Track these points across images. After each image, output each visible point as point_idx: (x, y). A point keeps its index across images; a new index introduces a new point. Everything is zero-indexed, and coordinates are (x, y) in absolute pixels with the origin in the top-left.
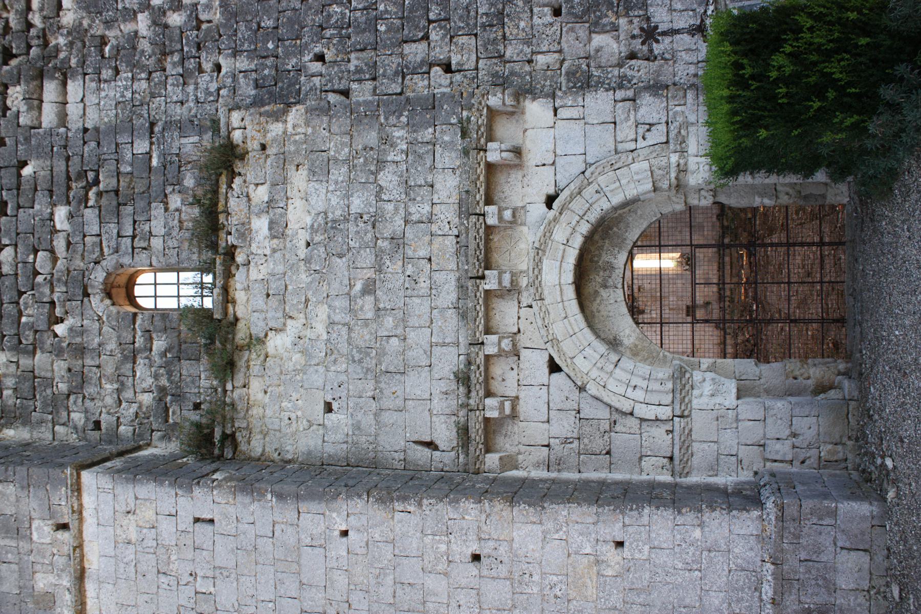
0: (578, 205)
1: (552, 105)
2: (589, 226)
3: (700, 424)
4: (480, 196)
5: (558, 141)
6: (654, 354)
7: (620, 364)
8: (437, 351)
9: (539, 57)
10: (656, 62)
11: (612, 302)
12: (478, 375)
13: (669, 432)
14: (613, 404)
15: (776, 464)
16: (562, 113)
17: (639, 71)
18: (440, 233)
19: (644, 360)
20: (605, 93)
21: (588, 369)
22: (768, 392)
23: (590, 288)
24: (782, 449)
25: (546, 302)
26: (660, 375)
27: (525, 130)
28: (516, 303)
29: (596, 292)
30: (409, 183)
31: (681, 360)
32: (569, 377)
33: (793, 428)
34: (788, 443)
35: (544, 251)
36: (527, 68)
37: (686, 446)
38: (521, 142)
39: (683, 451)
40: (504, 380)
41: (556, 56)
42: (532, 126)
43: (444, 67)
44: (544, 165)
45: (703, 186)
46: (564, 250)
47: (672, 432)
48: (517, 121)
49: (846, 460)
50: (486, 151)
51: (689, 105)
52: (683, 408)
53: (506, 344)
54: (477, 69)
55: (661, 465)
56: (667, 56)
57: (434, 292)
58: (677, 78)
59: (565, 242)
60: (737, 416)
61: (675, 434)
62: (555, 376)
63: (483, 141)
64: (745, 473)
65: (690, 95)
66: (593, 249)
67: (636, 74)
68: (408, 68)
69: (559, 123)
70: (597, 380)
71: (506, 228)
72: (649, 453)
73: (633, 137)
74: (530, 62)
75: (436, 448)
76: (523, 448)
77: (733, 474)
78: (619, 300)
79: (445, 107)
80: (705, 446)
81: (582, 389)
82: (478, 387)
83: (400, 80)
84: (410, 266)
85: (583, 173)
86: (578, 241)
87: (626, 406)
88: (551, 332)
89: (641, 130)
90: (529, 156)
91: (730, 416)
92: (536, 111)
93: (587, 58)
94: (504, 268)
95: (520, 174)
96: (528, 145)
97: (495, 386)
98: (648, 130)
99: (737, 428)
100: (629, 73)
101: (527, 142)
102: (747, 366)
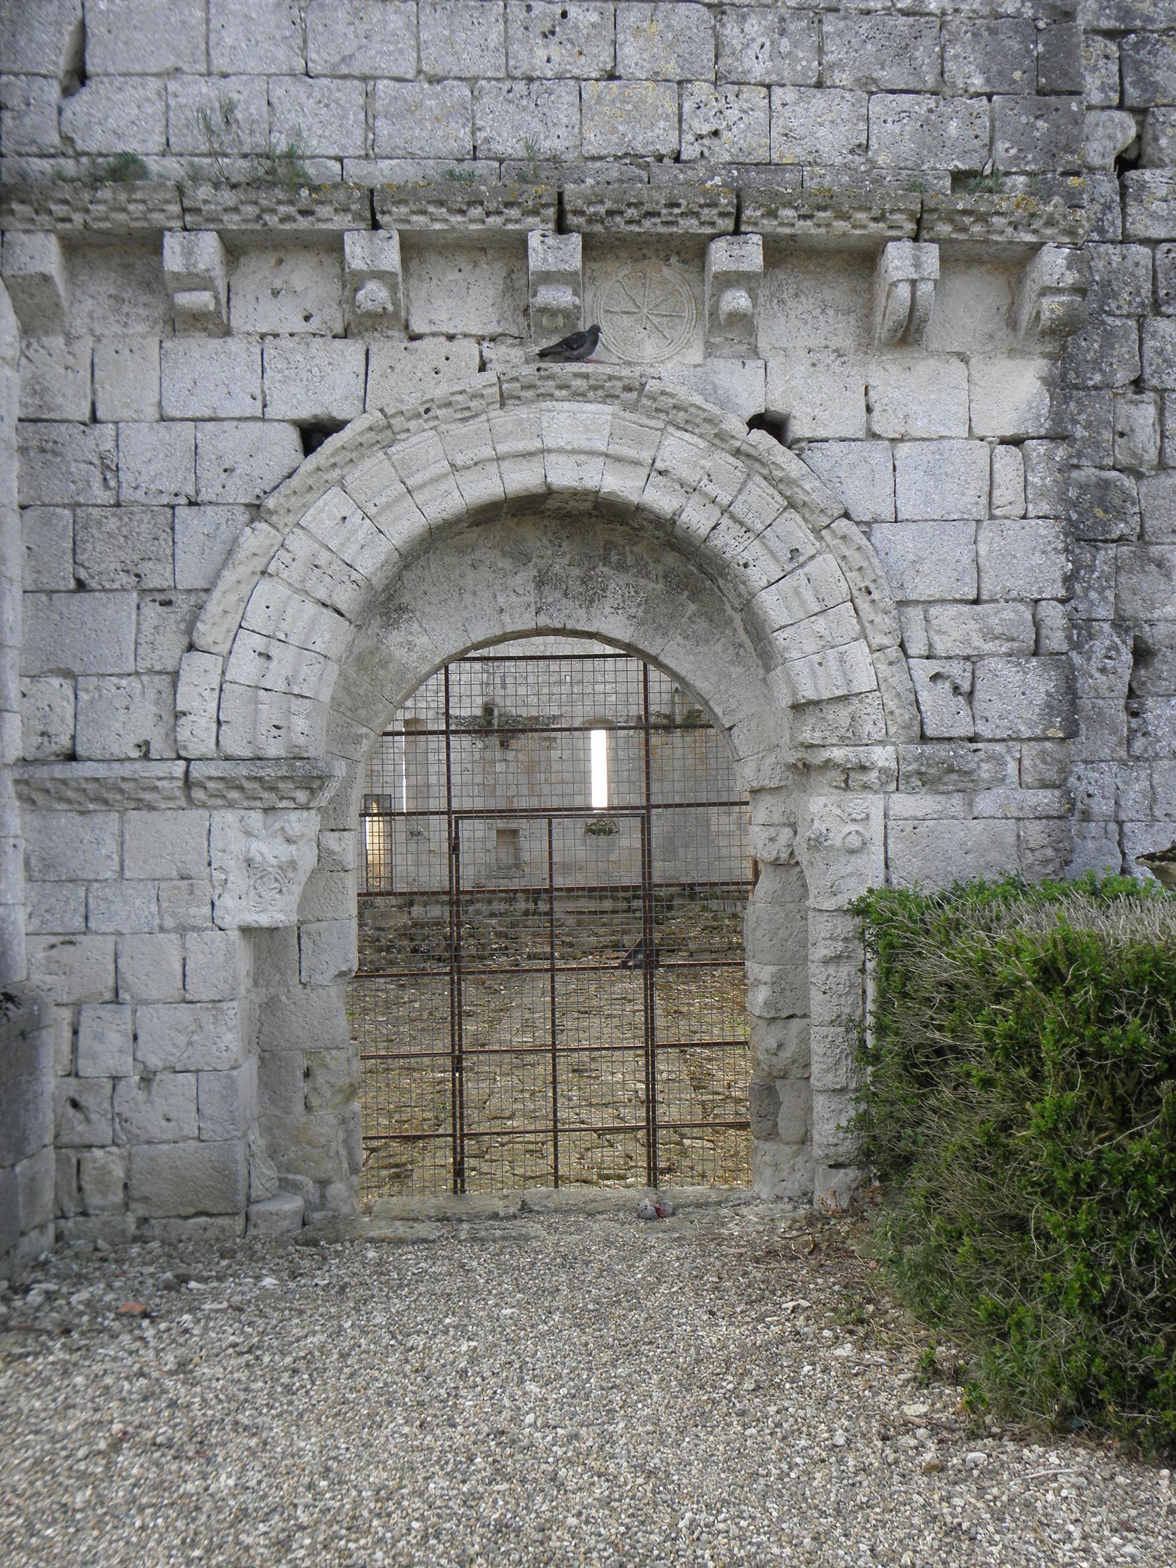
0: (760, 500)
1: (1032, 431)
2: (704, 531)
3: (172, 834)
4: (789, 222)
5: (933, 446)
6: (362, 713)
7: (329, 614)
8: (352, 93)
9: (1151, 411)
10: (1123, 716)
11: (501, 600)
12: (282, 209)
13: (145, 750)
14: (216, 594)
15: (67, 1034)
16: (1008, 458)
17: (1103, 670)
18: (688, 106)
19: (345, 685)
20: (1058, 575)
21: (312, 527)
22: (270, 1006)
23: (533, 538)
24: (108, 1050)
25: (495, 413)
26: (300, 724)
27: (964, 358)
28: (493, 329)
29: (523, 559)
30: (831, 17)
31: (349, 781)
32: (290, 476)
33: (167, 1077)
34: (126, 1065)
35: (633, 407)
36: (1122, 377)
37: (103, 797)
38: (934, 346)
39: (89, 786)
40: (276, 293)
41: (1152, 455)
42: (976, 377)
43: (1132, 155)
44: (869, 410)
45: (805, 833)
46: (636, 463)
47: (146, 756)
48: (991, 337)
49: (84, 1214)
50: (916, 239)
51: (1019, 795)
52: (211, 785)
53: (373, 295)
54: (1126, 240)
55: (52, 730)
56: (1139, 744)
57: (520, 87)
58: (1080, 768)
59: (659, 465)
60: (194, 928)
61: (138, 765)
62: (292, 438)
63: (945, 229)
64: (40, 955)
65: (1047, 799)
66: (640, 549)
67: (1095, 663)
68: (1136, 46)
69: (983, 451)
70: (284, 556)
71: (698, 301)
72: (84, 696)
73: (940, 648)
74: (1138, 384)
75: (67, 92)
76: (84, 347)
77: (36, 921)
78: (506, 618)
79: (1040, 123)
80: (110, 846)
81: (256, 510)
82: (251, 210)
83: (1105, 24)
84: (594, 17)
85: (846, 515)
86: (661, 500)
87: (206, 632)
88: (413, 425)
89: (956, 670)
90: (894, 369)
91: (193, 911)
92: (1017, 390)
93: (1141, 536)
94: (589, 296)
95: (845, 342)
96: (925, 367)
97: (257, 273)
98: (956, 689)
99: (162, 929)
100: (1099, 646)
101: (932, 363)
102: (341, 946)
